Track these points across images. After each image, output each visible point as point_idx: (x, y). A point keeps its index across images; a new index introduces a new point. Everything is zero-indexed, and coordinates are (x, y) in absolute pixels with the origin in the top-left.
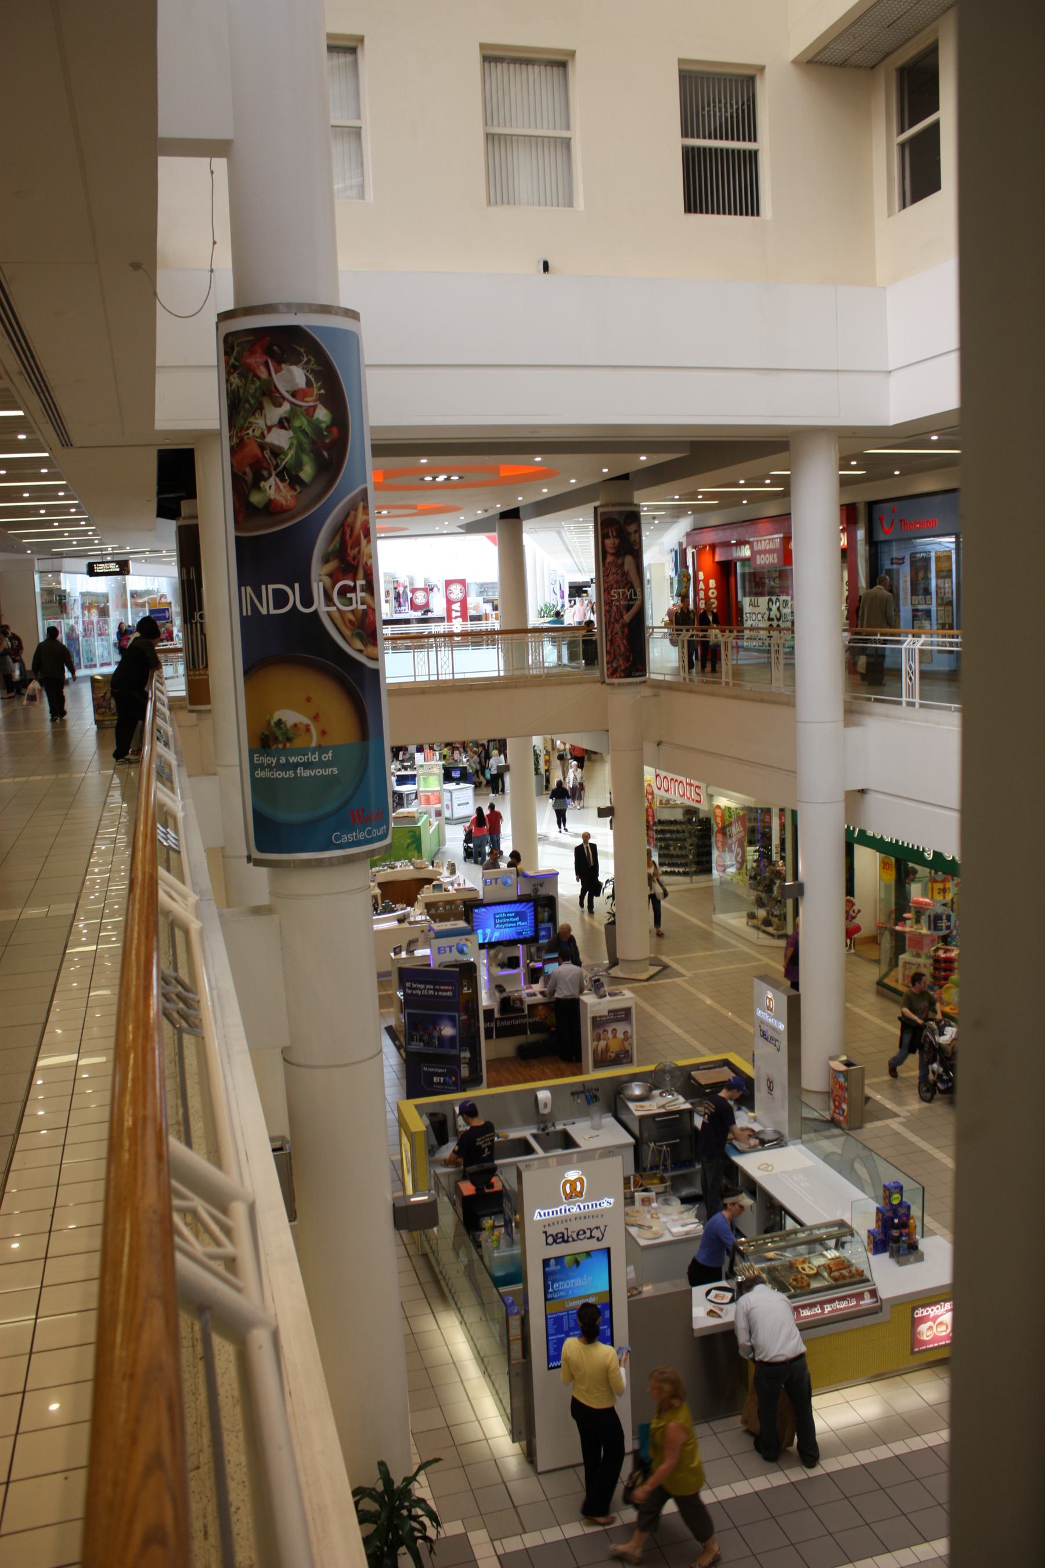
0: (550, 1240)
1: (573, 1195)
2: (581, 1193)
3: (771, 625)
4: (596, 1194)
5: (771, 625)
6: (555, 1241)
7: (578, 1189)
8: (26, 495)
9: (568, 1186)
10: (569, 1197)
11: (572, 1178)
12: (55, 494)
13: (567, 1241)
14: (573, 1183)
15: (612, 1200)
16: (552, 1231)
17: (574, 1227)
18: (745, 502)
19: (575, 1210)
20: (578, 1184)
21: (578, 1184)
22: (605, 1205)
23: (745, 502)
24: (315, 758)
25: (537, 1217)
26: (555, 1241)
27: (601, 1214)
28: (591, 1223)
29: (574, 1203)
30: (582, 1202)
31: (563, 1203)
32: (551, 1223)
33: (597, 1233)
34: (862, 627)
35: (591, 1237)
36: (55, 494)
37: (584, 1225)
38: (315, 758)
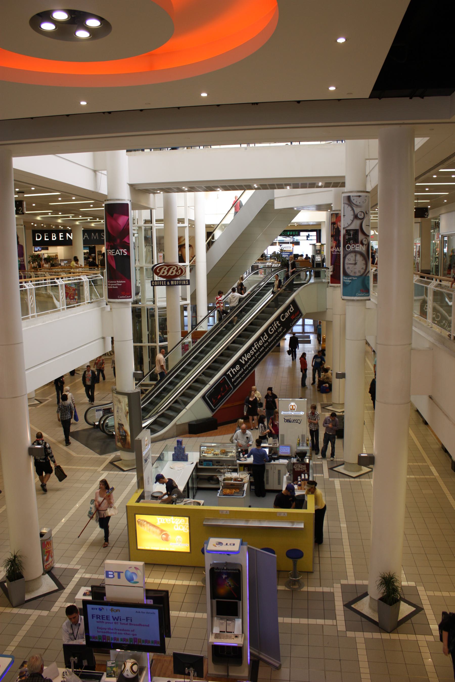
0: (286, 421)
1: (292, 410)
2: (295, 409)
3: (440, 281)
4: (298, 410)
5: (440, 281)
6: (287, 421)
7: (294, 408)
8: (427, 189)
9: (291, 406)
10: (291, 410)
11: (293, 405)
12: (439, 176)
13: (290, 422)
14: (292, 406)
15: (303, 413)
16: (286, 418)
17: (292, 418)
18: (34, 205)
19: (293, 413)
20: (294, 406)
21: (294, 406)
22: (301, 414)
23: (34, 205)
24: (266, 338)
25: (282, 413)
26: (287, 421)
27: (300, 416)
28: (297, 418)
29: (293, 412)
30: (295, 412)
31: (289, 411)
32: (286, 416)
33: (298, 421)
34: (441, 276)
35: (297, 422)
36: (439, 176)
37: (295, 418)
38: (266, 338)
